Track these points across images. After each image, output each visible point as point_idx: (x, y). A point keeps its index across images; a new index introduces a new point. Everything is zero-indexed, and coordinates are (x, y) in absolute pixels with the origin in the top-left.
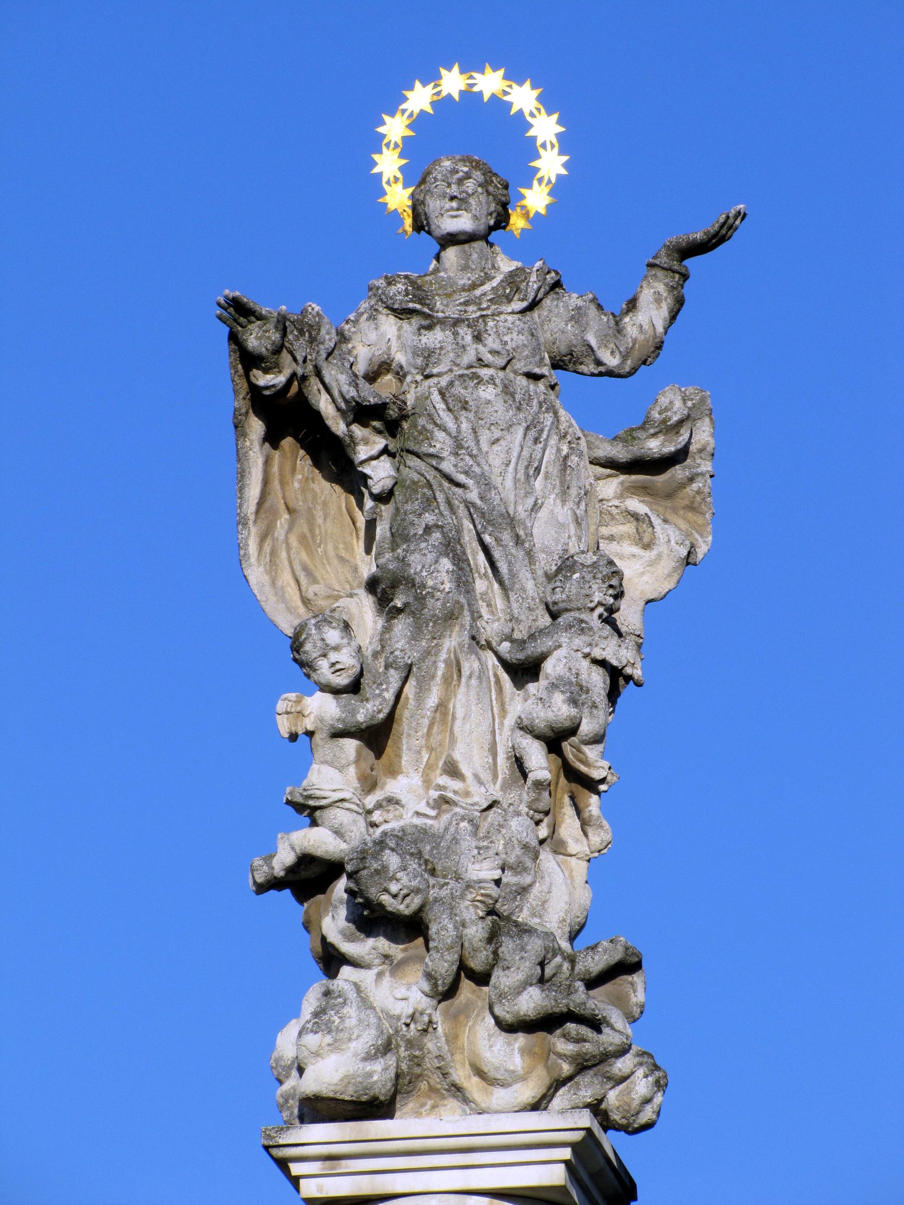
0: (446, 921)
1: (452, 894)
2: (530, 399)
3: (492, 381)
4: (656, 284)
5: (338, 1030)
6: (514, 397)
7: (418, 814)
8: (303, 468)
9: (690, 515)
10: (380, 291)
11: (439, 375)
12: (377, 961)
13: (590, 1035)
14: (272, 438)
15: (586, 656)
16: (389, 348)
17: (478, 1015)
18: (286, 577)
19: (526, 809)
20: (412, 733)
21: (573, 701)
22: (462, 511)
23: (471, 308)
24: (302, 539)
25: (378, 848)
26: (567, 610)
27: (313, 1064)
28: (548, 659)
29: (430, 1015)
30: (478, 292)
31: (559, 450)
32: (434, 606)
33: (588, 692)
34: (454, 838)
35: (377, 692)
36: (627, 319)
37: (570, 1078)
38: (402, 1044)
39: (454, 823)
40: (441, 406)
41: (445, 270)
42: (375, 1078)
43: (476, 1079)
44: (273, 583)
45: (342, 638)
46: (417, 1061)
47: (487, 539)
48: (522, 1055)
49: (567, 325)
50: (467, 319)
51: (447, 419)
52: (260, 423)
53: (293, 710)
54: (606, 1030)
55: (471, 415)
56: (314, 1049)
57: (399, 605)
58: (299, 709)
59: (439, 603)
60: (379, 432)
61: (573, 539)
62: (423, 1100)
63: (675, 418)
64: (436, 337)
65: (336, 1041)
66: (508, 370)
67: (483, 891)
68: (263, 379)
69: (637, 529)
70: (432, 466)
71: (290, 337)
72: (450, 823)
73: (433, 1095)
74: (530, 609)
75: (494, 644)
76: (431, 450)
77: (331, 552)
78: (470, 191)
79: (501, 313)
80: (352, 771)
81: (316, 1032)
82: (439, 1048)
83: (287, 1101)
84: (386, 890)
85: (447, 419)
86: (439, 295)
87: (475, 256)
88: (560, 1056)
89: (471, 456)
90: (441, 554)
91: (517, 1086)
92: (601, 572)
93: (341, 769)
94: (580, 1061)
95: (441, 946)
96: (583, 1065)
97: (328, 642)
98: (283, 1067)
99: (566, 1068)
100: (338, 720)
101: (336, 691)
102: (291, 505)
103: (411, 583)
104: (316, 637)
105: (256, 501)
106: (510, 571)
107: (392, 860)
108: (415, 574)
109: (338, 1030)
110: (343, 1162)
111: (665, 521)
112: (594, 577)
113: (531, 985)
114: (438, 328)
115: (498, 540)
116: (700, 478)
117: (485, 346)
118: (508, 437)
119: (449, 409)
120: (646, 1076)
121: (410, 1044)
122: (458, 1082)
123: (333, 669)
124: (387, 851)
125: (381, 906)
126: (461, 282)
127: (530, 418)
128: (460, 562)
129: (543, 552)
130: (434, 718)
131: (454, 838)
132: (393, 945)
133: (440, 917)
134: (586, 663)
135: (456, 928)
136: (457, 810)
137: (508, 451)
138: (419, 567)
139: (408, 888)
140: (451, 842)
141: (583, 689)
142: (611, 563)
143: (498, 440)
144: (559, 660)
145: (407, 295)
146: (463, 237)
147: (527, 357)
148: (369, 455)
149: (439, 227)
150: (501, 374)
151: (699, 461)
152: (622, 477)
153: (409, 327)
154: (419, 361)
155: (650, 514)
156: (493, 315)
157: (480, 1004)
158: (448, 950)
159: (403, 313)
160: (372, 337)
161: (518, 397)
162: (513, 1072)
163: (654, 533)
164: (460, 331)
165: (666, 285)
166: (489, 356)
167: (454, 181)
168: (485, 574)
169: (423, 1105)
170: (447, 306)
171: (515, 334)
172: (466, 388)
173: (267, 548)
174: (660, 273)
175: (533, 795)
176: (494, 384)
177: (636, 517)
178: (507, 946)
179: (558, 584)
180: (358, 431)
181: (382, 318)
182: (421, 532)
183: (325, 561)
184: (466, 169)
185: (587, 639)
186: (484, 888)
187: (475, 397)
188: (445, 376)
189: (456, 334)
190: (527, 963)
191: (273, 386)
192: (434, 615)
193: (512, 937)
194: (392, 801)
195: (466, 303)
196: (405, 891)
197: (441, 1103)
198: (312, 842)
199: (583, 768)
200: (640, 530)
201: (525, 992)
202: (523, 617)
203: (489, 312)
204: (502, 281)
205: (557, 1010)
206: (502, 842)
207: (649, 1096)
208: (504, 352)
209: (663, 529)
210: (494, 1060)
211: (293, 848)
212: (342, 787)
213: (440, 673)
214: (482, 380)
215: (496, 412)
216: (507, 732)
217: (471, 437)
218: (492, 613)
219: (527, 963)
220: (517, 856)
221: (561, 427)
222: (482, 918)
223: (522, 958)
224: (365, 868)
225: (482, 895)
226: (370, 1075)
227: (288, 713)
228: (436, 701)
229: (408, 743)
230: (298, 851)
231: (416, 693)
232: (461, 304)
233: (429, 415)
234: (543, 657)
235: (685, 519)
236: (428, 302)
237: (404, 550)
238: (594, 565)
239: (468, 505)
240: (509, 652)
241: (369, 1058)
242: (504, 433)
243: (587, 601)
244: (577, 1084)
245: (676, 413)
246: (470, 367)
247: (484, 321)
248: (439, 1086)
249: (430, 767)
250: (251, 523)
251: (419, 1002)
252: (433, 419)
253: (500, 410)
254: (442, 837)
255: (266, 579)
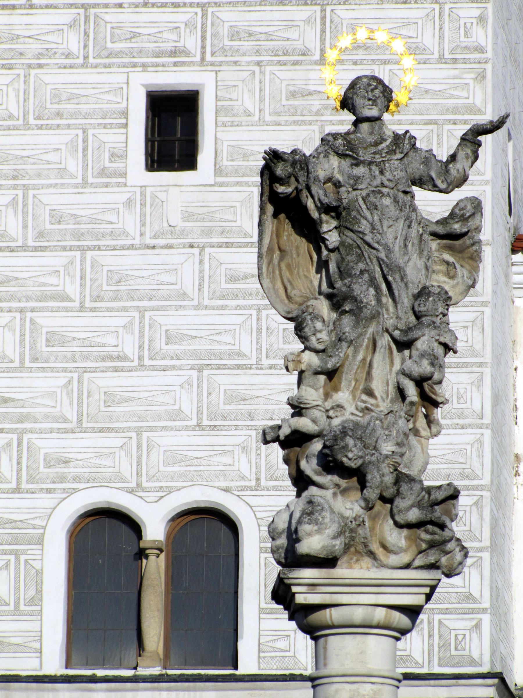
0: (376, 473)
1: (378, 459)
2: (406, 205)
3: (388, 195)
4: (466, 149)
5: (321, 524)
6: (398, 204)
7: (352, 414)
8: (288, 229)
9: (470, 262)
10: (330, 143)
11: (361, 190)
12: (332, 486)
13: (439, 532)
14: (275, 215)
15: (437, 340)
16: (333, 172)
17: (384, 518)
18: (279, 284)
19: (404, 414)
20: (349, 372)
21: (432, 364)
22: (375, 261)
23: (377, 156)
24: (289, 266)
25: (343, 435)
26: (426, 316)
27: (306, 539)
28: (418, 341)
29: (363, 518)
30: (380, 147)
31: (418, 231)
32: (367, 312)
33: (438, 359)
34: (373, 429)
35: (337, 353)
36: (451, 166)
37: (424, 551)
38: (348, 531)
39: (373, 421)
40: (364, 206)
41: (361, 133)
42: (337, 548)
43: (381, 549)
44: (274, 288)
45: (323, 326)
46: (352, 538)
47: (390, 278)
48: (405, 540)
49: (420, 166)
50: (375, 162)
51: (367, 213)
52: (272, 207)
53: (296, 359)
54: (446, 529)
55: (379, 213)
56: (308, 532)
57: (347, 309)
58: (298, 359)
59: (369, 311)
60: (333, 217)
61: (423, 276)
62: (351, 556)
63: (468, 214)
64: (360, 171)
65: (319, 529)
66: (394, 189)
67: (394, 460)
68: (281, 189)
69: (447, 269)
70: (360, 237)
71: (296, 170)
72: (370, 421)
73: (357, 554)
74: (406, 313)
75: (390, 330)
76: (360, 229)
77: (301, 273)
78: (377, 96)
79: (391, 160)
80: (321, 391)
81: (310, 524)
82: (365, 534)
83: (278, 549)
84: (346, 456)
85: (367, 213)
86: (360, 148)
87: (377, 128)
88: (422, 540)
89: (379, 233)
90: (369, 286)
91: (402, 554)
92: (442, 297)
93: (316, 390)
94: (432, 543)
95: (373, 486)
96: (432, 545)
97: (317, 328)
98: (277, 533)
99: (424, 546)
100: (319, 367)
101: (317, 352)
102: (283, 247)
103: (355, 299)
104: (311, 326)
105: (267, 246)
106: (399, 294)
107: (350, 441)
108: (357, 295)
109: (321, 524)
110: (318, 587)
111: (462, 266)
112: (439, 300)
113: (414, 507)
114: (361, 166)
115: (394, 279)
116: (477, 244)
117: (385, 177)
118: (396, 225)
119: (368, 209)
120: (460, 551)
121: (351, 531)
122: (373, 550)
123: (318, 342)
124: (348, 437)
125: (342, 463)
126: (369, 140)
127: (406, 215)
128: (377, 289)
129: (412, 283)
130: (359, 366)
131: (373, 429)
132: (341, 480)
133: (373, 472)
134: (436, 344)
135: (380, 477)
136: (373, 414)
137: (396, 232)
138: (359, 292)
139: (357, 456)
140: (372, 431)
141: (436, 358)
142: (446, 292)
143: (391, 226)
144: (424, 342)
145: (344, 146)
146: (373, 119)
147: (404, 183)
148: (329, 229)
149: (361, 113)
150: (392, 191)
151: (474, 234)
152: (439, 241)
153: (346, 163)
154: (352, 182)
155: (455, 262)
156: (388, 160)
157: (384, 512)
158: (376, 488)
159: (342, 156)
160: (326, 166)
161: (400, 204)
162: (401, 548)
163: (456, 272)
164: (372, 168)
165: (472, 150)
166: (387, 182)
167: (370, 90)
168: (386, 295)
169: (351, 559)
170: (365, 154)
171: (399, 171)
172: (376, 198)
173: (271, 269)
174: (469, 144)
175: (408, 408)
176: (390, 197)
177: (448, 263)
178: (404, 487)
179: (422, 302)
180: (324, 217)
181: (331, 157)
182: (358, 273)
183: (298, 277)
184: (375, 84)
185: (437, 332)
186: (394, 458)
187: (381, 203)
188: (364, 190)
189: (370, 169)
190: (413, 497)
191: (286, 193)
192: (366, 317)
193: (406, 483)
194: (340, 407)
195: (374, 153)
196: (356, 457)
197: (361, 559)
198: (301, 425)
199: (433, 396)
200: (449, 269)
201: (411, 511)
202: (403, 317)
203: (386, 159)
204: (391, 142)
205: (426, 520)
206: (395, 432)
207: (461, 561)
208: (394, 181)
209: (461, 270)
210: (392, 541)
211: (290, 427)
212: (318, 399)
213: (365, 344)
214: (384, 194)
215: (391, 211)
216: (394, 375)
217: (379, 224)
218: (388, 314)
219: (413, 497)
220: (402, 439)
221: (418, 219)
222: (392, 473)
223: (411, 494)
224: (337, 445)
225: (393, 462)
226: (334, 546)
227: (293, 361)
228: (362, 357)
229: (345, 376)
230: (293, 428)
231: (353, 354)
232: (372, 153)
233: (358, 211)
234: (416, 339)
235: (468, 264)
236: (355, 151)
237: (349, 281)
238: (439, 293)
239: (379, 259)
240: (399, 336)
241: (335, 538)
242: (395, 222)
243: (436, 312)
244: (428, 553)
245: (468, 211)
246: (377, 187)
247: (384, 164)
248: (361, 551)
249: (355, 389)
250: (264, 256)
251: (359, 511)
252: (359, 213)
253: (392, 211)
254: (367, 428)
255: (270, 285)
